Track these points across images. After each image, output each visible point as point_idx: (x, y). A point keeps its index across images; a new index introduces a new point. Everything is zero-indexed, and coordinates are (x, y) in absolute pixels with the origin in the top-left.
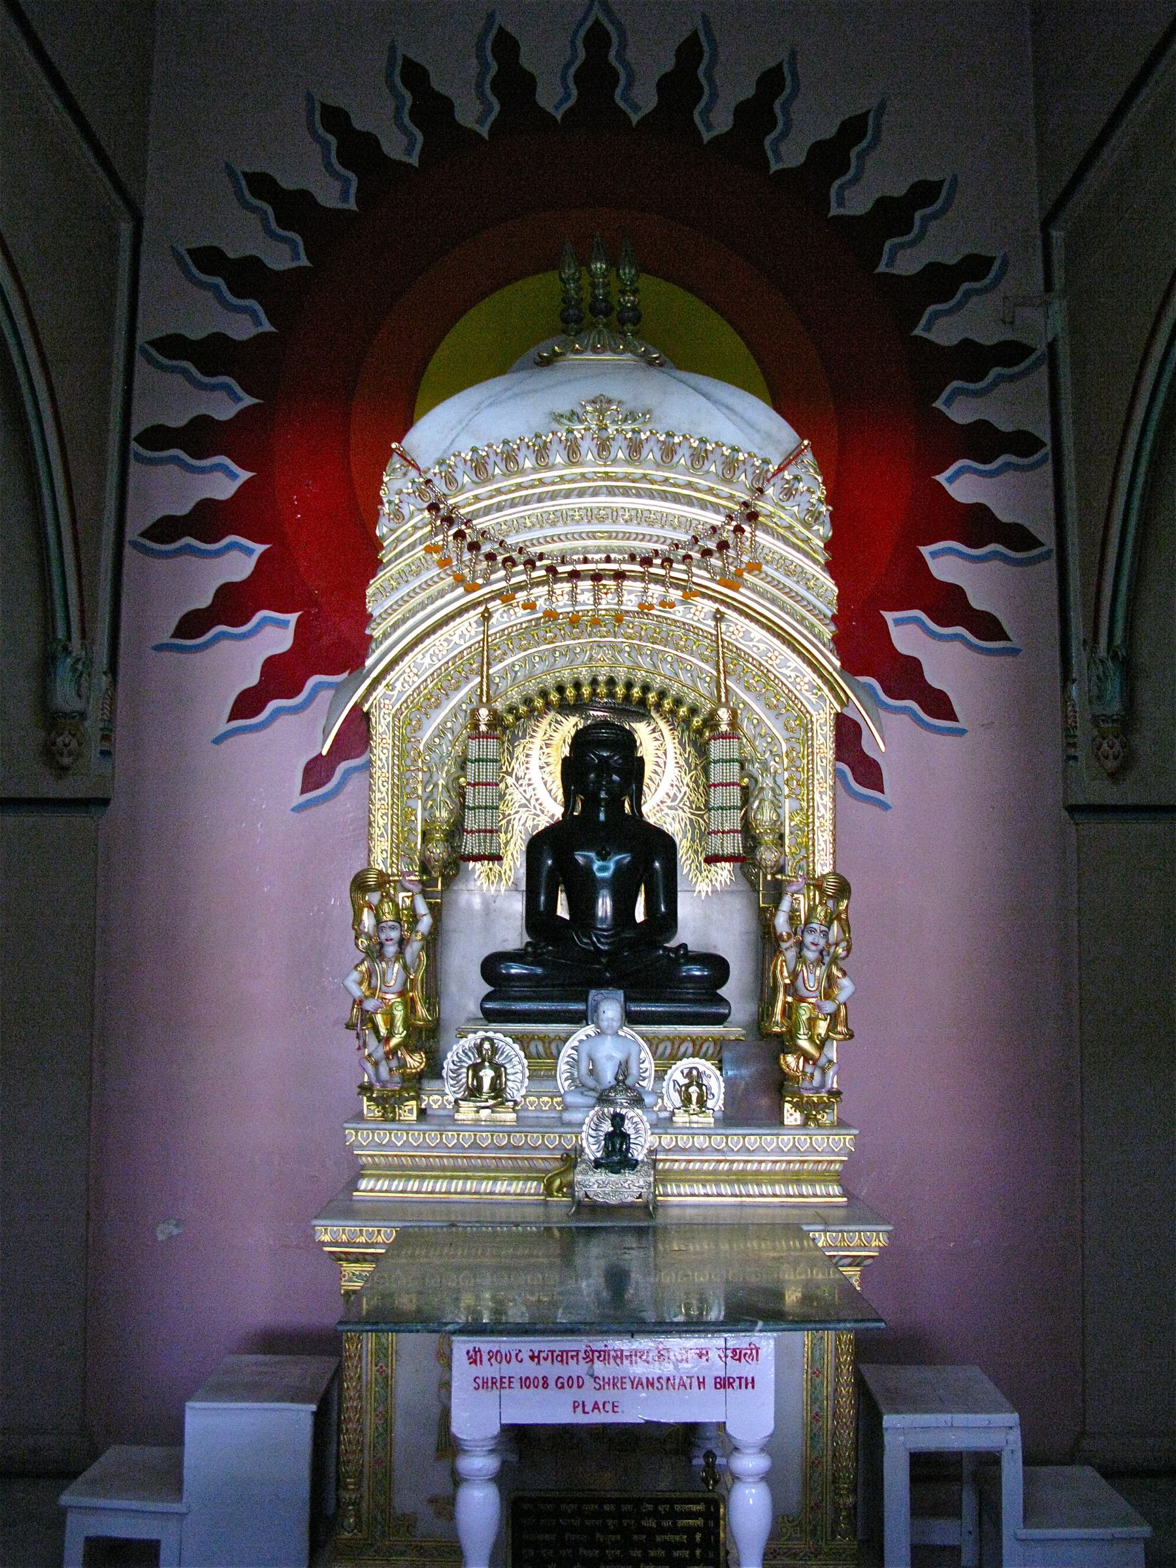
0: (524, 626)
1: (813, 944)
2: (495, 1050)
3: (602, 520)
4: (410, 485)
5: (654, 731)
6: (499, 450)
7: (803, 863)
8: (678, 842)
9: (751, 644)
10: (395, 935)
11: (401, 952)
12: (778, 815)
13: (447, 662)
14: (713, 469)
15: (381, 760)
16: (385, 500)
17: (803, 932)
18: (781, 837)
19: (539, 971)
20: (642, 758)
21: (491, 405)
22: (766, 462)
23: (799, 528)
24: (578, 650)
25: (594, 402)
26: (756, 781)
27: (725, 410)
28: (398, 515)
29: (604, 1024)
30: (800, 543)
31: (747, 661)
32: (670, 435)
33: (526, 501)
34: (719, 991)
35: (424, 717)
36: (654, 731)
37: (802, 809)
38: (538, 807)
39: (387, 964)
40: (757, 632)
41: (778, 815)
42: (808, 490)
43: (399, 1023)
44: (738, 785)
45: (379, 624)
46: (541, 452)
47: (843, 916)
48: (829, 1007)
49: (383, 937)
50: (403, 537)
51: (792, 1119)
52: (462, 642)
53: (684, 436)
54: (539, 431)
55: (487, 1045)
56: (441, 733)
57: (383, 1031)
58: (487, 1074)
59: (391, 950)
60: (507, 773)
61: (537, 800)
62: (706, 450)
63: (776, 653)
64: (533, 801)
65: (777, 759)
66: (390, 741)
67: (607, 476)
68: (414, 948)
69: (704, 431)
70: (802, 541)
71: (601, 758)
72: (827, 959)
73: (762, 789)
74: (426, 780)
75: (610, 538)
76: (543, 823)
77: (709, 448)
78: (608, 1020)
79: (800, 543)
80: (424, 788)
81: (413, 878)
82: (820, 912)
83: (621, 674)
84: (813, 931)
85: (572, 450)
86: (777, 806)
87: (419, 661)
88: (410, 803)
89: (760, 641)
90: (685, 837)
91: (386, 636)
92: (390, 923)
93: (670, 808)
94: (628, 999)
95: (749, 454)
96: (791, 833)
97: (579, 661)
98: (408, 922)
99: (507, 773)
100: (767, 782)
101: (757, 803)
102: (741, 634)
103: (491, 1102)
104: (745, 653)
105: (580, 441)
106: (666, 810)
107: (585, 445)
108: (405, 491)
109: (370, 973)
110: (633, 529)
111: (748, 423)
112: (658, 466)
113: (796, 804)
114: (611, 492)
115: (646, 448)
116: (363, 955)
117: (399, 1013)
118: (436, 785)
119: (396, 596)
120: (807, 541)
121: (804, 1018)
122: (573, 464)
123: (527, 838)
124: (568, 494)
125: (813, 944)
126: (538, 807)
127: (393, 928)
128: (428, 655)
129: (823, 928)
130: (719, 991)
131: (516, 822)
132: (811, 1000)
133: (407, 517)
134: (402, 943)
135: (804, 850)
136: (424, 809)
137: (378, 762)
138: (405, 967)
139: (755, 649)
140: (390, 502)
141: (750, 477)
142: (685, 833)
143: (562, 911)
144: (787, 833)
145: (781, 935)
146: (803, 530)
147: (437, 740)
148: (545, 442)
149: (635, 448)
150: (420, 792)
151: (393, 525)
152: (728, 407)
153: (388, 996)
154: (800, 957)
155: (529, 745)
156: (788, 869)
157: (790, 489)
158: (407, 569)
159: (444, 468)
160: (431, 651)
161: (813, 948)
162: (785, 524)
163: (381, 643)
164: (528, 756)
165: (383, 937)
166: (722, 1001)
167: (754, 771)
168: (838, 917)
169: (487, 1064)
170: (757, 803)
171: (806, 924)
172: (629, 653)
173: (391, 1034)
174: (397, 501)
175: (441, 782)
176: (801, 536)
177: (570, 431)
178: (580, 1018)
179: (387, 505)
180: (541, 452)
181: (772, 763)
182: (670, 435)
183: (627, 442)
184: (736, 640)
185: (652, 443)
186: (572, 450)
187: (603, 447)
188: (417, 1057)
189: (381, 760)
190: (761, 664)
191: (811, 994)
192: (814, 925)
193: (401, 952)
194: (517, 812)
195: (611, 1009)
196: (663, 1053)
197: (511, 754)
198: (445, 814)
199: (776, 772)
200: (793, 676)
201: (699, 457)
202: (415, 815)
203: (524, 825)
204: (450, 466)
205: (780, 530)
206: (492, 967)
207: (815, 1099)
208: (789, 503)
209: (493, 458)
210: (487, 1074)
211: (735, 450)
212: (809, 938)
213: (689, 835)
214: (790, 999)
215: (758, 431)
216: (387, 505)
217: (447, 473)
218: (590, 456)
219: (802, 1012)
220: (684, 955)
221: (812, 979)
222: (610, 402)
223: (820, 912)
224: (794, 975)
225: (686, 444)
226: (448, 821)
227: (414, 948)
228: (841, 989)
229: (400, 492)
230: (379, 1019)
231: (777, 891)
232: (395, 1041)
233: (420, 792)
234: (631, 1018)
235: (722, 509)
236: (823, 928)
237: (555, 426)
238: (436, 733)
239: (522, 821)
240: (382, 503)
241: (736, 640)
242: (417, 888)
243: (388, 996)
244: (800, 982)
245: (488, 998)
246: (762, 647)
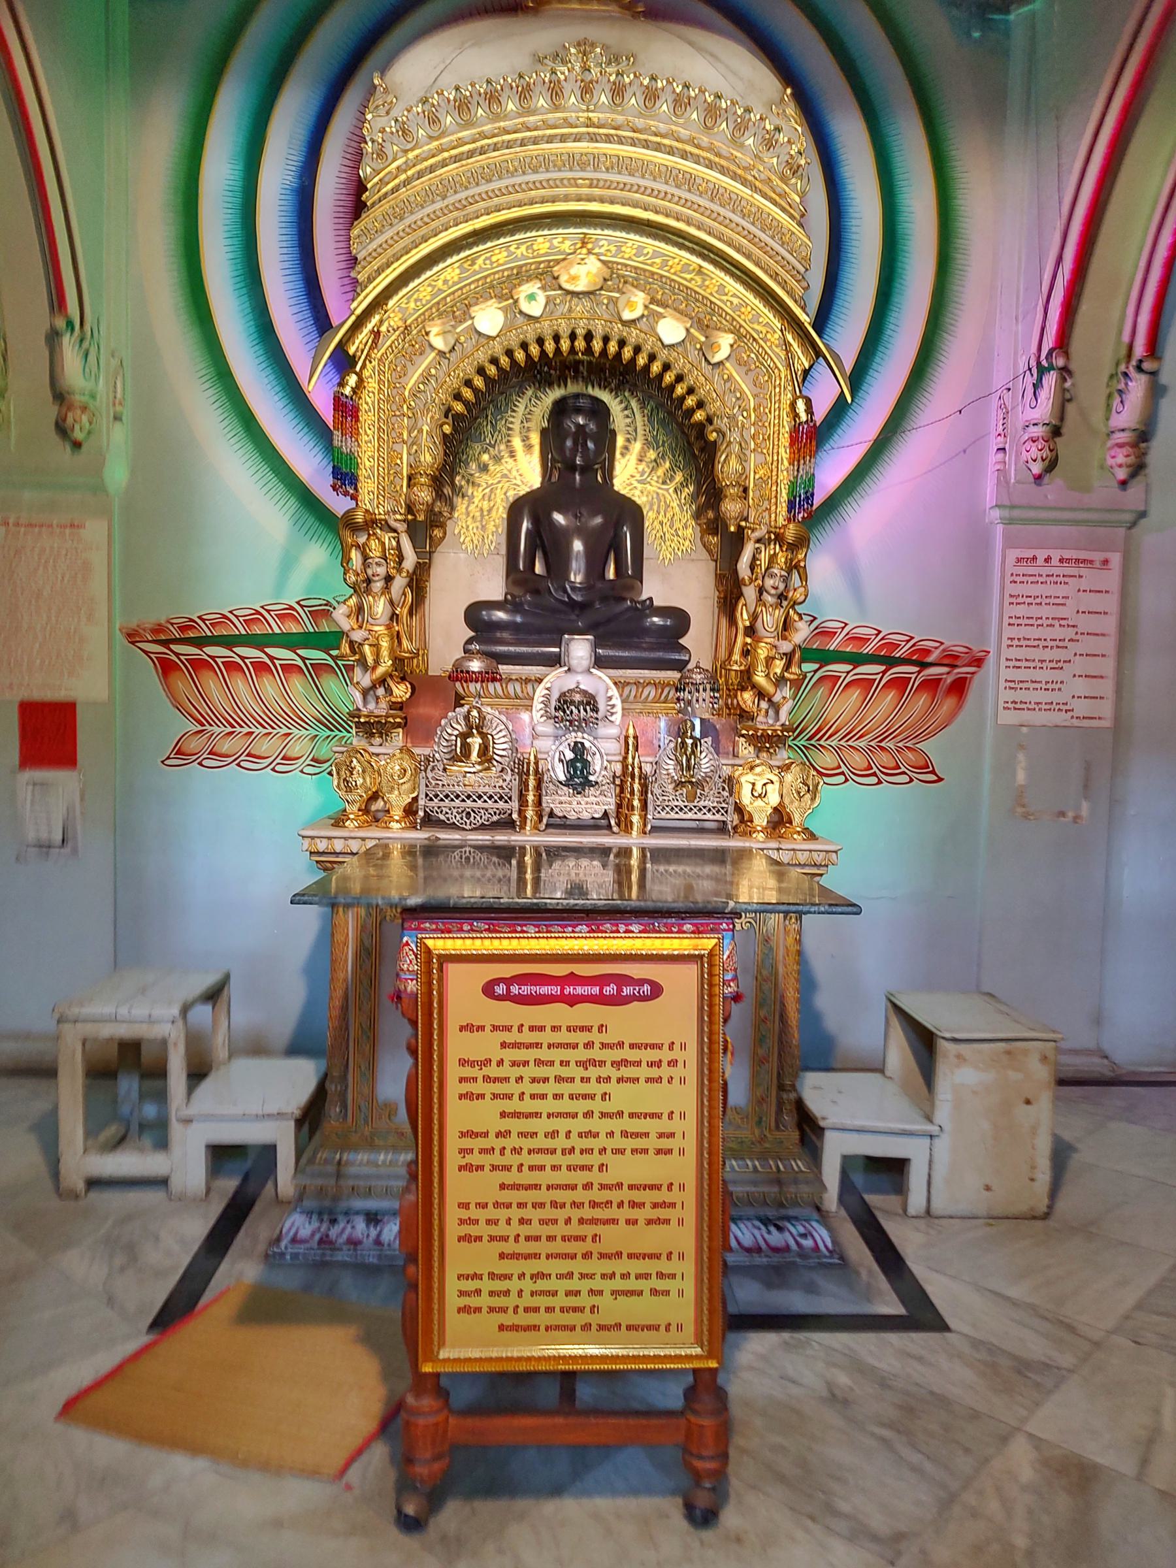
0: (506, 274)
2: (482, 718)
3: (583, 167)
4: (393, 123)
5: (626, 408)
6: (482, 91)
7: (766, 514)
10: (381, 571)
11: (387, 588)
12: (744, 468)
13: (431, 308)
15: (367, 403)
18: (745, 490)
19: (519, 619)
21: (473, 45)
22: (748, 110)
23: (776, 181)
24: (558, 301)
25: (579, 44)
26: (724, 435)
27: (708, 57)
28: (381, 154)
30: (777, 198)
32: (653, 78)
33: (509, 145)
34: (681, 641)
35: (408, 364)
36: (626, 408)
40: (734, 286)
41: (744, 468)
42: (789, 141)
43: (385, 653)
44: (451, 1411)
46: (525, 93)
48: (786, 647)
49: (370, 572)
50: (386, 180)
51: (746, 752)
52: (445, 287)
53: (668, 82)
54: (523, 70)
55: (475, 713)
56: (426, 378)
57: (370, 660)
58: (476, 742)
59: (378, 586)
60: (490, 444)
62: (689, 98)
63: (749, 309)
64: (514, 473)
65: (745, 414)
66: (376, 386)
67: (590, 123)
68: (399, 582)
70: (780, 195)
71: (578, 425)
72: (785, 603)
73: (730, 443)
75: (590, 186)
76: (523, 490)
77: (692, 94)
79: (777, 198)
81: (398, 517)
82: (781, 559)
83: (599, 331)
84: (772, 576)
85: (555, 91)
86: (742, 459)
89: (734, 295)
90: (651, 509)
91: (370, 280)
92: (377, 560)
93: (639, 482)
94: (596, 645)
95: (732, 102)
96: (755, 485)
98: (395, 561)
99: (490, 444)
100: (734, 436)
101: (723, 457)
103: (478, 767)
104: (719, 307)
105: (563, 83)
106: (636, 484)
107: (567, 87)
108: (388, 129)
109: (360, 609)
110: (613, 177)
112: (640, 115)
113: (761, 458)
114: (593, 138)
115: (630, 91)
116: (352, 591)
117: (385, 644)
119: (381, 239)
120: (784, 195)
121: (762, 657)
122: (557, 108)
123: (507, 506)
124: (550, 139)
126: (518, 478)
130: (681, 641)
132: (768, 640)
134: (389, 579)
135: (766, 503)
136: (409, 454)
137: (365, 406)
138: (391, 602)
140: (373, 141)
141: (731, 126)
142: (652, 505)
143: (539, 568)
144: (752, 485)
146: (780, 183)
148: (528, 84)
149: (618, 91)
151: (378, 165)
152: (712, 55)
153: (376, 628)
154: (760, 599)
155: (511, 419)
156: (751, 519)
157: (770, 140)
158: (390, 211)
159: (427, 107)
160: (415, 296)
161: (773, 591)
162: (763, 177)
163: (366, 287)
165: (370, 572)
166: (683, 648)
168: (797, 567)
170: (723, 457)
171: (766, 570)
173: (377, 662)
174: (380, 140)
175: (425, 428)
176: (778, 190)
177: (553, 72)
178: (554, 661)
179: (370, 144)
180: (525, 93)
181: (741, 418)
182: (653, 78)
183: (610, 85)
184: (711, 294)
185: (634, 88)
186: (555, 91)
187: (586, 90)
188: (402, 687)
189: (367, 403)
190: (734, 319)
191: (769, 635)
192: (776, 571)
193: (387, 588)
195: (580, 649)
196: (628, 696)
198: (429, 459)
199: (743, 426)
201: (681, 103)
202: (401, 459)
204: (434, 106)
205: (757, 183)
206: (474, 615)
208: (769, 155)
209: (476, 97)
210: (476, 742)
213: (655, 508)
214: (749, 640)
215: (741, 79)
216: (370, 144)
217: (430, 112)
218: (573, 99)
219: (760, 651)
220: (649, 607)
222: (593, 45)
223: (781, 559)
224: (754, 617)
226: (432, 467)
227: (399, 582)
229: (383, 131)
231: (736, 541)
232: (381, 670)
234: (600, 663)
240: (366, 143)
242: (401, 527)
243: (376, 628)
245: (469, 641)
246: (736, 301)
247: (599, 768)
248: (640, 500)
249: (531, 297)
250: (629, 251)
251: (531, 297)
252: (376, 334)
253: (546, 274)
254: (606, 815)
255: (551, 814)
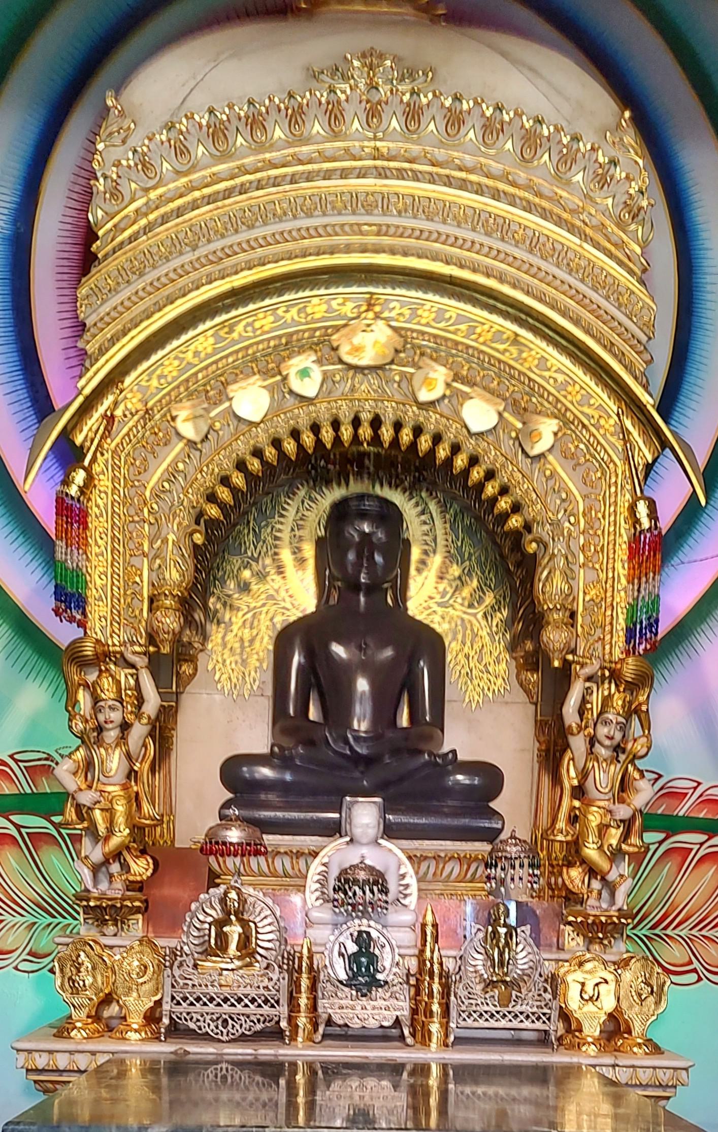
0: (272, 343)
1: (608, 737)
2: (242, 901)
4: (130, 155)
6: (242, 114)
8: (447, 644)
9: (547, 374)
10: (116, 716)
11: (123, 738)
12: (571, 587)
13: (178, 387)
14: (509, 145)
15: (98, 506)
16: (99, 174)
17: (595, 725)
18: (573, 615)
19: (288, 777)
20: (408, 540)
22: (576, 138)
23: (612, 227)
24: (338, 378)
27: (526, 71)
28: (115, 193)
29: (357, 832)
30: (613, 249)
31: (542, 396)
33: (276, 182)
37: (599, 581)
38: (288, 599)
39: (106, 750)
40: (558, 359)
41: (571, 587)
42: (627, 177)
43: (120, 820)
45: (95, 336)
46: (296, 116)
47: (644, 708)
48: (623, 812)
50: (122, 225)
51: (573, 944)
55: (233, 895)
56: (172, 475)
57: (102, 829)
58: (234, 931)
60: (252, 558)
61: (287, 591)
62: (502, 123)
63: (577, 387)
64: (283, 593)
65: (572, 519)
66: (110, 484)
67: (377, 155)
68: (139, 731)
69: (499, 96)
70: (615, 245)
71: (363, 534)
72: (622, 757)
73: (553, 556)
74: (153, 533)
75: (378, 234)
77: (506, 118)
78: (362, 826)
79: (613, 249)
80: (151, 544)
82: (618, 702)
84: (606, 723)
85: (334, 114)
86: (569, 576)
87: (143, 383)
88: (135, 561)
89: (558, 371)
90: (454, 638)
91: (102, 351)
92: (111, 703)
94: (386, 809)
96: (585, 609)
97: (339, 393)
98: (132, 704)
99: (252, 558)
100: (559, 548)
102: (536, 362)
103: (238, 963)
104: (540, 385)
105: (344, 104)
107: (349, 110)
108: (124, 162)
109: (89, 764)
110: (407, 222)
111: (555, 89)
112: (441, 145)
113: (592, 575)
114: (382, 174)
116: (79, 741)
117: (120, 808)
118: (165, 541)
119: (115, 301)
120: (620, 245)
121: (594, 824)
122: (336, 136)
124: (328, 175)
125: (608, 737)
126: (288, 599)
127: (111, 708)
128: (155, 376)
129: (621, 719)
131: (263, 616)
132: (602, 804)
133: (127, 199)
134: (125, 727)
135: (599, 631)
136: (151, 569)
137: (95, 509)
138: (128, 756)
139: (551, 381)
140: (105, 177)
141: (555, 158)
142: (455, 633)
143: (314, 713)
144: (581, 609)
145: (570, 726)
146: (616, 229)
147: (166, 485)
148: (300, 106)
149: (413, 114)
150: (146, 549)
151: (112, 207)
152: (531, 69)
153: (110, 789)
154: (591, 752)
156: (580, 652)
157: (604, 176)
158: (127, 265)
159: (173, 134)
160: (158, 372)
161: (607, 742)
162: (595, 222)
163: (97, 360)
164: (277, 538)
165: (101, 718)
167: (544, 534)
168: (637, 711)
169: (233, 918)
171: (599, 715)
172: (399, 383)
173: (110, 831)
174: (114, 176)
175: (171, 537)
176: (614, 239)
177: (332, 91)
178: (333, 830)
179: (101, 180)
180: (296, 116)
181: (567, 524)
182: (457, 98)
184: (530, 369)
185: (434, 110)
186: (334, 114)
187: (373, 112)
188: (142, 862)
189: (98, 506)
190: (558, 400)
191: (602, 796)
192: (611, 717)
193: (123, 738)
194: (264, 605)
195: (365, 814)
197: (257, 535)
198: (175, 575)
199: (570, 535)
200: (596, 416)
201: (492, 129)
202: (141, 576)
203: (271, 619)
204: (181, 133)
205: (588, 230)
206: (233, 771)
207: (603, 919)
208: (603, 194)
209: (235, 122)
210: (234, 931)
211: (539, 121)
212: (603, 731)
213: (460, 637)
214: (577, 804)
215: (567, 99)
216: (101, 180)
218: (356, 124)
219: (591, 817)
220: (452, 762)
221: (603, 778)
223: (618, 702)
224: (584, 775)
225: (476, 112)
226: (179, 586)
227: (139, 731)
228: (637, 791)
229: (118, 164)
230: (98, 815)
232: (115, 841)
233: (146, 549)
234: (390, 832)
235: (518, 201)
236: (621, 719)
237: (314, 84)
238: (166, 476)
239: (270, 615)
241: (530, 369)
243: (110, 789)
244: (590, 783)
245: (226, 805)
246: (560, 378)
247: (391, 963)
248: (441, 627)
249: (304, 373)
250: (426, 315)
251: (304, 373)
252: (110, 419)
253: (323, 344)
254: (397, 1022)
255: (329, 1022)
